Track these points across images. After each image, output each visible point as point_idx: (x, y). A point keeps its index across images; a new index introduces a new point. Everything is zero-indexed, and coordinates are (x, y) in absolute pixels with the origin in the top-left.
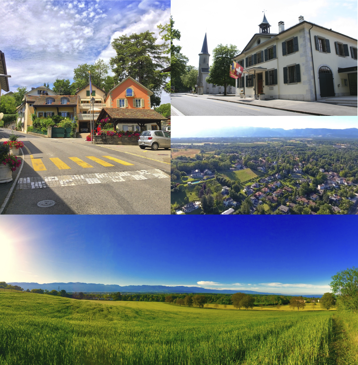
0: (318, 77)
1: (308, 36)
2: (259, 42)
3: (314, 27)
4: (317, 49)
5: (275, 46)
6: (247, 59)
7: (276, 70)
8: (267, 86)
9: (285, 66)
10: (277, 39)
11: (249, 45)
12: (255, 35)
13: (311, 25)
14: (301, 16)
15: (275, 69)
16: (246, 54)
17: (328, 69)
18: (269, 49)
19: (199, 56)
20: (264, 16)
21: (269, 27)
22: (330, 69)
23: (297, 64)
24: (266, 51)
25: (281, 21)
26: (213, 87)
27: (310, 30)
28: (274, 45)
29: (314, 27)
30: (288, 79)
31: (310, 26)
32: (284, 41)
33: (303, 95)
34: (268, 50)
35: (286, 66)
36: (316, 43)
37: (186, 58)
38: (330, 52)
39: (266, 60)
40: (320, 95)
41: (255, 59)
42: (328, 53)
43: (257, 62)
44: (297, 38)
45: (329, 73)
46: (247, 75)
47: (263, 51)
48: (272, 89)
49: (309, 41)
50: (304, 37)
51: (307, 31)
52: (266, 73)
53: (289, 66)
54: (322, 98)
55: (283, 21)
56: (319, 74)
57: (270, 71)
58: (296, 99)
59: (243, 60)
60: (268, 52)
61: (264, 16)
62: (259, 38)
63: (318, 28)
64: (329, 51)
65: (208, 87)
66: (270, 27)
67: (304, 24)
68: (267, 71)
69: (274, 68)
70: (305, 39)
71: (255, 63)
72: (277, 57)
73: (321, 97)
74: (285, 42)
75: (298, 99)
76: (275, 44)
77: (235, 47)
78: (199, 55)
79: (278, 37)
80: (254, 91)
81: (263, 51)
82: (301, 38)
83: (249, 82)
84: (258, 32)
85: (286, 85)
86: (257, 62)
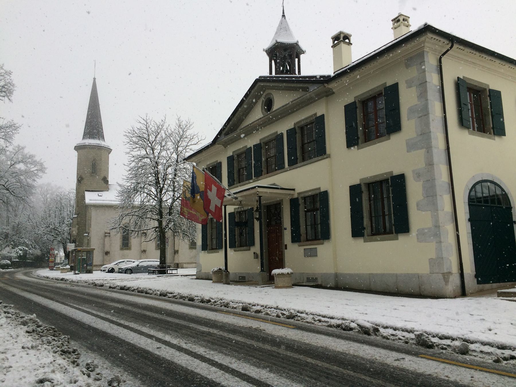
0: (468, 216)
1: (433, 79)
2: (269, 104)
3: (456, 46)
4: (462, 123)
5: (323, 116)
6: (230, 160)
7: (326, 193)
8: (296, 245)
9: (356, 181)
10: (329, 94)
11: (235, 119)
12: (257, 81)
13: (446, 42)
14: (401, 15)
15: (322, 190)
16: (226, 145)
17: (499, 192)
18: (302, 128)
19: (76, 153)
20: (95, 79)
21: (298, 57)
22: (503, 190)
23: (396, 172)
24: (291, 133)
25: (341, 33)
26: (122, 249)
27: (443, 59)
28: (319, 115)
29: (456, 46)
30: (366, 222)
31: (445, 44)
32: (349, 99)
33: (419, 276)
34: (298, 131)
35: (357, 182)
36: (462, 101)
37: (35, 163)
38: (504, 134)
39: (293, 163)
40: (476, 276)
41: (258, 160)
42: (497, 138)
43: (264, 170)
44: (395, 87)
45: (499, 202)
46: (233, 211)
47: (282, 134)
48: (313, 253)
49: (438, 95)
50: (423, 84)
51: (431, 61)
52: (294, 203)
53: (367, 181)
54: (481, 286)
55: (347, 31)
56: (469, 205)
57: (305, 198)
58: (416, 291)
59: (220, 163)
60: (298, 136)
61: (95, 79)
62: (267, 92)
63: (468, 50)
64: (475, 130)
65: (107, 249)
66: (302, 56)
67: (422, 39)
68: (296, 196)
69: (319, 188)
70: (425, 91)
71: (259, 175)
72: (328, 152)
73: (479, 283)
74: (354, 103)
75: (373, 287)
76: (319, 110)
77: (188, 126)
78: (78, 148)
79: (333, 85)
80: (158, 252)
81: (282, 134)
82: (409, 87)
83: (241, 234)
84: (266, 73)
85: (360, 241)
86: (264, 170)
